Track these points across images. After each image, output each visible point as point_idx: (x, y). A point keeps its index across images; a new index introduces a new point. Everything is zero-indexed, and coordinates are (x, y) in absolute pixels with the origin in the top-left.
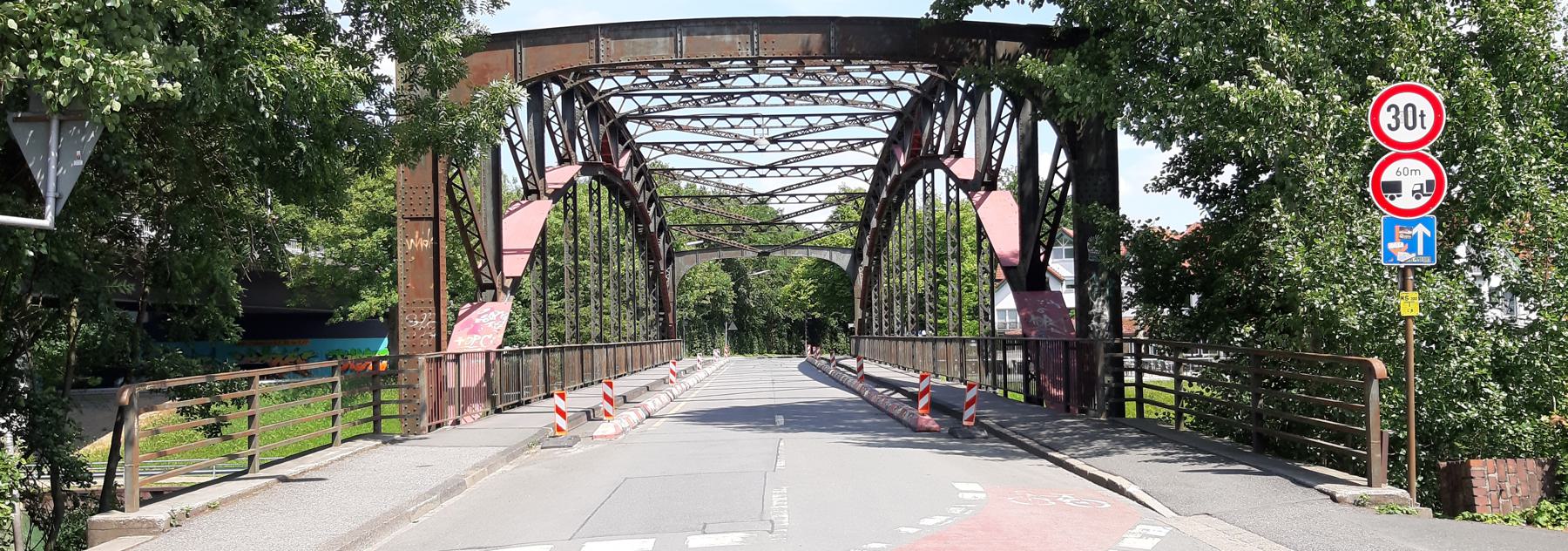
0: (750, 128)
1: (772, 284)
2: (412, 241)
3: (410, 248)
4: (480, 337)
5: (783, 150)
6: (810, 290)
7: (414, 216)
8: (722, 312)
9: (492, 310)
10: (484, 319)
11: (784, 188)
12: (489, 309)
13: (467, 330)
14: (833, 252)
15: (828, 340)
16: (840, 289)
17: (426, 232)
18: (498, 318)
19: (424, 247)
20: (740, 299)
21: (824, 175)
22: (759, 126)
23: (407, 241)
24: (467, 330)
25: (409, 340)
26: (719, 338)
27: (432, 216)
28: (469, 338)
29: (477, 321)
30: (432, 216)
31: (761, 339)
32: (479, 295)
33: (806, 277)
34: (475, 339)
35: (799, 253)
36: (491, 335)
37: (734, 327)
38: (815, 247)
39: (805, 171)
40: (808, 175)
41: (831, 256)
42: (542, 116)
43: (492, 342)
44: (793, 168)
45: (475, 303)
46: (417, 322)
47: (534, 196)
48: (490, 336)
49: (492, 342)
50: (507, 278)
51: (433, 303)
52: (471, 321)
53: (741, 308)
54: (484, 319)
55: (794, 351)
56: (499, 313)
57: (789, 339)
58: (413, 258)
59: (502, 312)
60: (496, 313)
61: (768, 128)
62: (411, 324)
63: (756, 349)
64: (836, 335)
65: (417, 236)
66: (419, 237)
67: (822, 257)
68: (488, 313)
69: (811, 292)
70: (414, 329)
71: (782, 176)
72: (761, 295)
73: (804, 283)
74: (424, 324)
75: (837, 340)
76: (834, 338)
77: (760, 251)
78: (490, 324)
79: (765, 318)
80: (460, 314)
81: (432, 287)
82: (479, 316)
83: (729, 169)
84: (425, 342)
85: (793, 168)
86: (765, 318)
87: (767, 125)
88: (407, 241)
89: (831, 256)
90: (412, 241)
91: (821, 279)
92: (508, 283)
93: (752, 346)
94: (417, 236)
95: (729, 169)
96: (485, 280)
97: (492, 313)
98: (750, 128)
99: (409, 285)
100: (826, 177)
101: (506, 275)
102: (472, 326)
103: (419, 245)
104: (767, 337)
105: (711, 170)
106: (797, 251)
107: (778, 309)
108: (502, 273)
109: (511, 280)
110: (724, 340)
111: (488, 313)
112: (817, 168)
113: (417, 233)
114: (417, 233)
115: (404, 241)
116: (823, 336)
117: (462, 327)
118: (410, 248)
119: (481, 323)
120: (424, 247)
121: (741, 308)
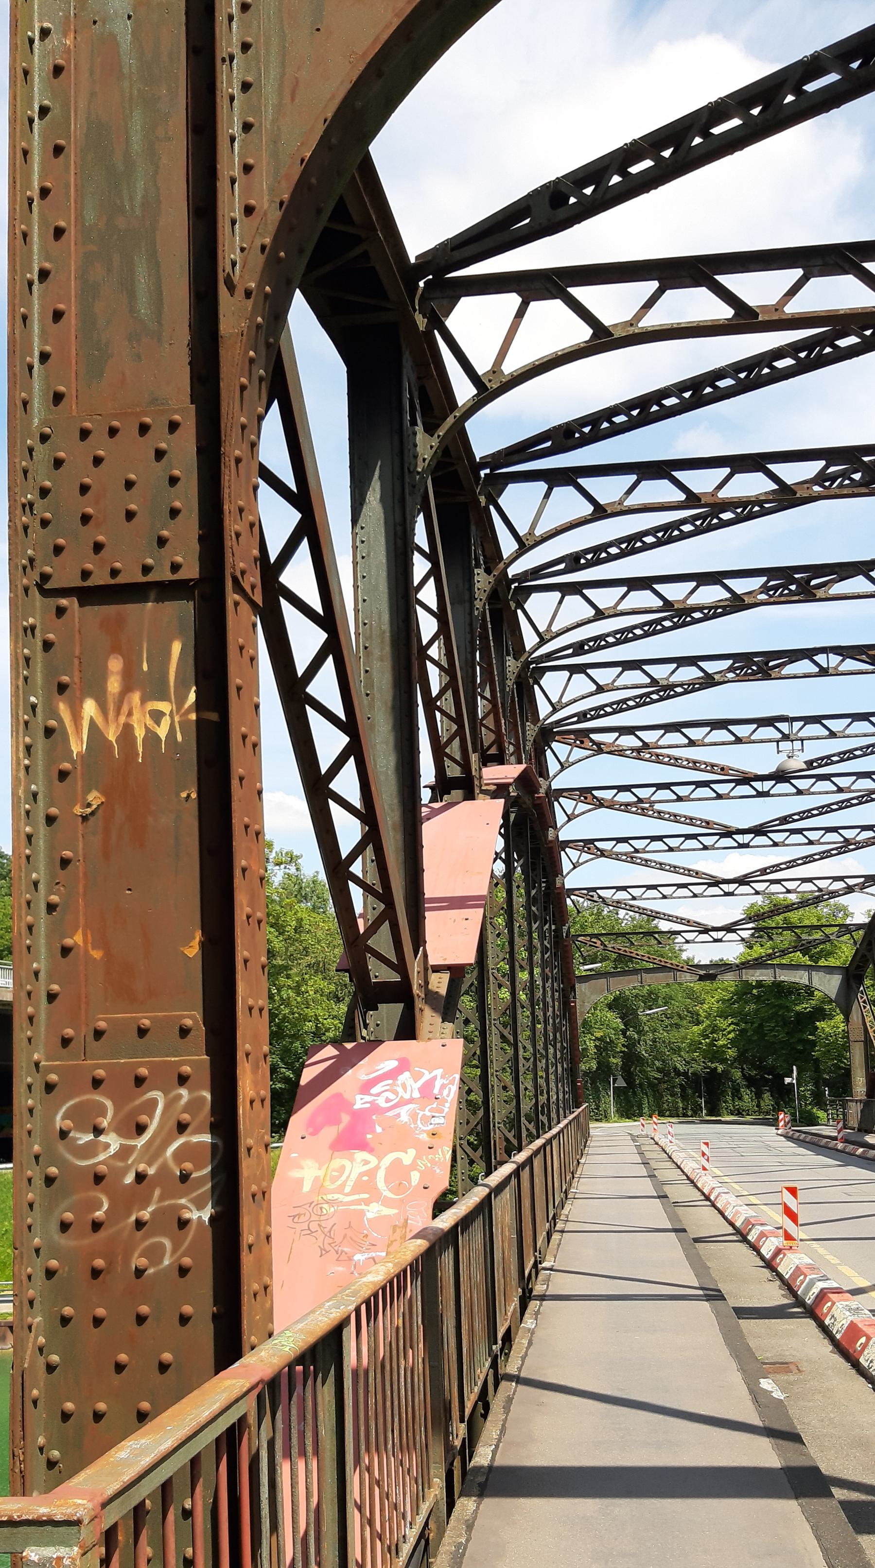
0: (770, 741)
1: (667, 1027)
2: (90, 708)
3: (78, 746)
4: (373, 1161)
5: (800, 792)
6: (729, 1033)
7: (100, 578)
8: (608, 1062)
9: (404, 1065)
10: (382, 1096)
11: (765, 869)
12: (393, 1064)
13: (330, 1133)
14: (814, 973)
15: (729, 1098)
16: (771, 1031)
17: (161, 658)
18: (426, 1090)
19: (151, 738)
20: (631, 1044)
21: (847, 842)
22: (786, 737)
23: (63, 709)
24: (330, 1133)
25: (64, 1241)
26: (604, 1097)
27: (191, 571)
28: (337, 1163)
29: (360, 1102)
30: (191, 571)
31: (651, 1099)
32: (358, 1021)
33: (723, 1015)
34: (359, 1169)
35: (761, 975)
36: (412, 1152)
37: (621, 1083)
38: (782, 966)
39: (813, 835)
40: (818, 842)
41: (810, 979)
42: (471, 613)
43: (415, 1177)
44: (793, 832)
45: (349, 1046)
46: (113, 1142)
47: (457, 794)
48: (408, 1157)
49: (415, 1177)
50: (437, 969)
51: (200, 1033)
52: (344, 1105)
53: (631, 1058)
54: (382, 1096)
55: (690, 1113)
56: (427, 1076)
57: (684, 1097)
58: (95, 798)
59: (439, 1072)
60: (416, 1077)
61: (802, 740)
62: (90, 1150)
63: (646, 1110)
64: (738, 1091)
65: (114, 685)
66: (127, 689)
67: (797, 980)
68: (392, 1075)
69: (731, 1036)
70: (98, 1179)
71: (664, 897)
72: (654, 1041)
73: (722, 1023)
74: (154, 1151)
75: (740, 1099)
76: (737, 1094)
77: (702, 972)
78: (404, 1113)
79: (659, 1070)
80: (303, 1081)
81: (193, 950)
82: (366, 1088)
83: (688, 837)
84: (154, 1254)
85: (793, 832)
86: (659, 1070)
87: (800, 735)
88: (63, 709)
89: (810, 979)
90: (90, 708)
91: (743, 1017)
92: (440, 983)
93: (640, 1107)
94: (114, 685)
95: (688, 837)
96: (380, 973)
97: (405, 1077)
98: (770, 741)
99: (77, 939)
100: (847, 846)
101: (432, 961)
102: (346, 1119)
103: (128, 730)
104: (658, 1097)
105: (660, 838)
106: (758, 972)
107: (676, 1058)
108: (425, 956)
109: (445, 977)
110: (610, 1102)
111: (392, 1075)
112: (834, 830)
113: (115, 664)
114: (115, 664)
115: (54, 713)
116: (724, 1093)
117: (315, 1128)
118: (78, 746)
119: (375, 1109)
120: (151, 738)
121: (631, 1058)
